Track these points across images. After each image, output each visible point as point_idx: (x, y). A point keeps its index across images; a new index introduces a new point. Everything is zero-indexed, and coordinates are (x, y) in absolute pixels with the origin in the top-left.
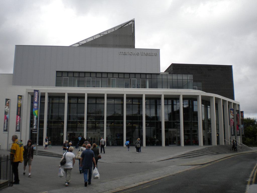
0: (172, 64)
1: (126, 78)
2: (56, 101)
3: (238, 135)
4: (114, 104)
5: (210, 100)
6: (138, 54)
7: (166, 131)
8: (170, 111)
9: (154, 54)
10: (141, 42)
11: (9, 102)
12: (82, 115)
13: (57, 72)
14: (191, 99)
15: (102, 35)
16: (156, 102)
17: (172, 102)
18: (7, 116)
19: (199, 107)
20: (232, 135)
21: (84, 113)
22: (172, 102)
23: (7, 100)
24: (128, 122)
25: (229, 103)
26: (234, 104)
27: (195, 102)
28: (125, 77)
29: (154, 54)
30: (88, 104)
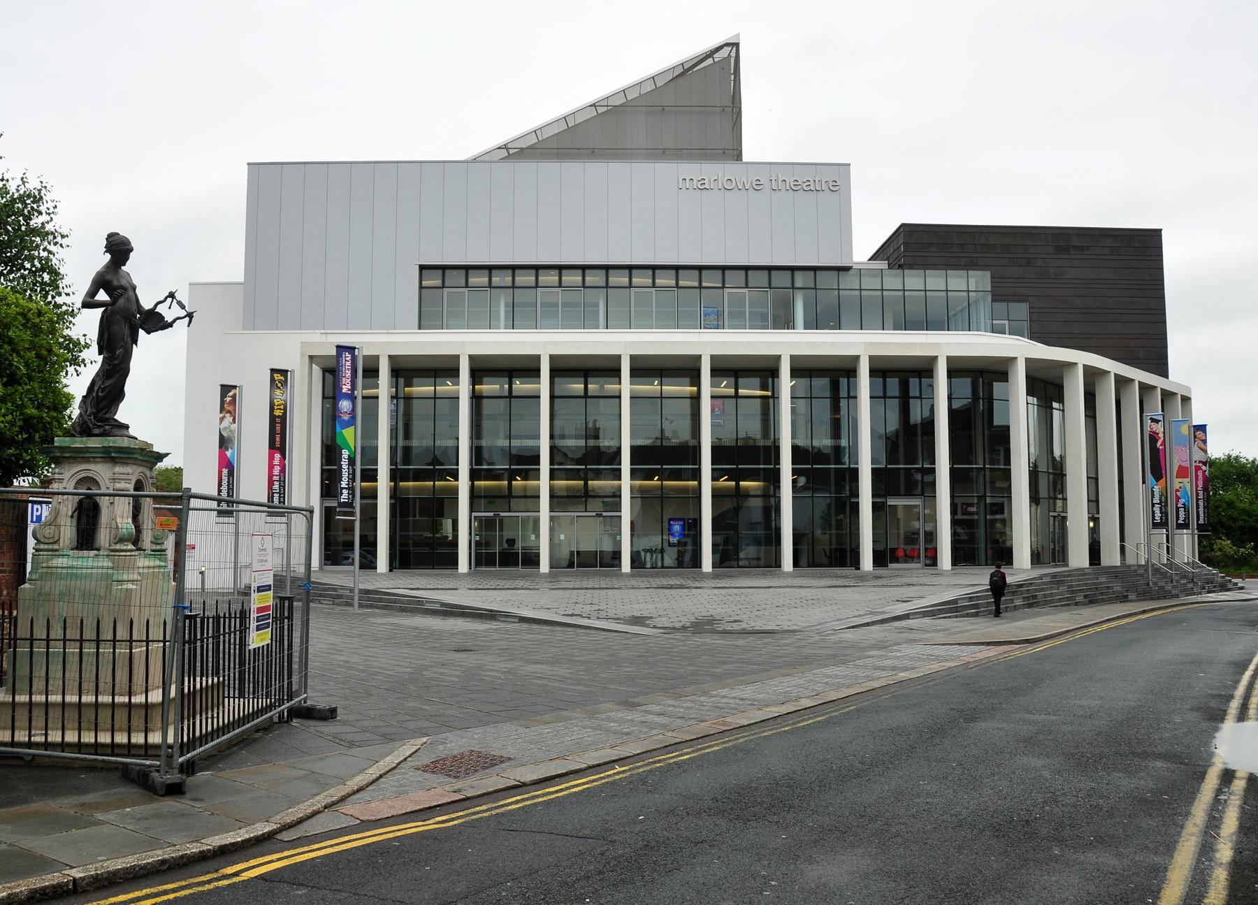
0: (903, 225)
1: (787, 288)
2: (422, 389)
3: (1179, 526)
4: (435, 398)
5: (1062, 378)
6: (758, 187)
7: (876, 508)
8: (893, 424)
9: (827, 185)
10: (763, 138)
11: (234, 397)
12: (530, 443)
13: (422, 268)
14: (982, 376)
15: (601, 110)
16: (835, 387)
17: (905, 387)
18: (228, 453)
19: (1019, 412)
20: (1155, 525)
21: (537, 437)
22: (905, 387)
23: (226, 389)
24: (677, 475)
25: (1145, 389)
26: (1167, 395)
27: (997, 387)
28: (704, 284)
29: (827, 185)
30: (552, 397)
